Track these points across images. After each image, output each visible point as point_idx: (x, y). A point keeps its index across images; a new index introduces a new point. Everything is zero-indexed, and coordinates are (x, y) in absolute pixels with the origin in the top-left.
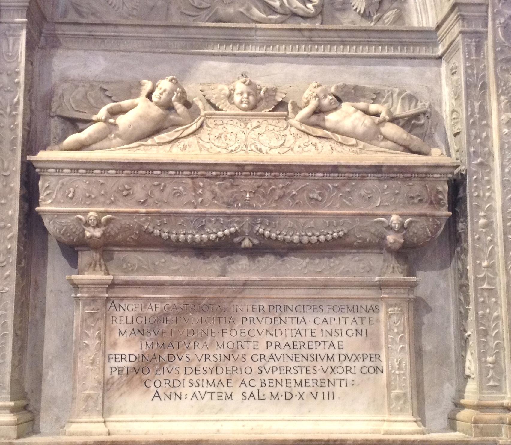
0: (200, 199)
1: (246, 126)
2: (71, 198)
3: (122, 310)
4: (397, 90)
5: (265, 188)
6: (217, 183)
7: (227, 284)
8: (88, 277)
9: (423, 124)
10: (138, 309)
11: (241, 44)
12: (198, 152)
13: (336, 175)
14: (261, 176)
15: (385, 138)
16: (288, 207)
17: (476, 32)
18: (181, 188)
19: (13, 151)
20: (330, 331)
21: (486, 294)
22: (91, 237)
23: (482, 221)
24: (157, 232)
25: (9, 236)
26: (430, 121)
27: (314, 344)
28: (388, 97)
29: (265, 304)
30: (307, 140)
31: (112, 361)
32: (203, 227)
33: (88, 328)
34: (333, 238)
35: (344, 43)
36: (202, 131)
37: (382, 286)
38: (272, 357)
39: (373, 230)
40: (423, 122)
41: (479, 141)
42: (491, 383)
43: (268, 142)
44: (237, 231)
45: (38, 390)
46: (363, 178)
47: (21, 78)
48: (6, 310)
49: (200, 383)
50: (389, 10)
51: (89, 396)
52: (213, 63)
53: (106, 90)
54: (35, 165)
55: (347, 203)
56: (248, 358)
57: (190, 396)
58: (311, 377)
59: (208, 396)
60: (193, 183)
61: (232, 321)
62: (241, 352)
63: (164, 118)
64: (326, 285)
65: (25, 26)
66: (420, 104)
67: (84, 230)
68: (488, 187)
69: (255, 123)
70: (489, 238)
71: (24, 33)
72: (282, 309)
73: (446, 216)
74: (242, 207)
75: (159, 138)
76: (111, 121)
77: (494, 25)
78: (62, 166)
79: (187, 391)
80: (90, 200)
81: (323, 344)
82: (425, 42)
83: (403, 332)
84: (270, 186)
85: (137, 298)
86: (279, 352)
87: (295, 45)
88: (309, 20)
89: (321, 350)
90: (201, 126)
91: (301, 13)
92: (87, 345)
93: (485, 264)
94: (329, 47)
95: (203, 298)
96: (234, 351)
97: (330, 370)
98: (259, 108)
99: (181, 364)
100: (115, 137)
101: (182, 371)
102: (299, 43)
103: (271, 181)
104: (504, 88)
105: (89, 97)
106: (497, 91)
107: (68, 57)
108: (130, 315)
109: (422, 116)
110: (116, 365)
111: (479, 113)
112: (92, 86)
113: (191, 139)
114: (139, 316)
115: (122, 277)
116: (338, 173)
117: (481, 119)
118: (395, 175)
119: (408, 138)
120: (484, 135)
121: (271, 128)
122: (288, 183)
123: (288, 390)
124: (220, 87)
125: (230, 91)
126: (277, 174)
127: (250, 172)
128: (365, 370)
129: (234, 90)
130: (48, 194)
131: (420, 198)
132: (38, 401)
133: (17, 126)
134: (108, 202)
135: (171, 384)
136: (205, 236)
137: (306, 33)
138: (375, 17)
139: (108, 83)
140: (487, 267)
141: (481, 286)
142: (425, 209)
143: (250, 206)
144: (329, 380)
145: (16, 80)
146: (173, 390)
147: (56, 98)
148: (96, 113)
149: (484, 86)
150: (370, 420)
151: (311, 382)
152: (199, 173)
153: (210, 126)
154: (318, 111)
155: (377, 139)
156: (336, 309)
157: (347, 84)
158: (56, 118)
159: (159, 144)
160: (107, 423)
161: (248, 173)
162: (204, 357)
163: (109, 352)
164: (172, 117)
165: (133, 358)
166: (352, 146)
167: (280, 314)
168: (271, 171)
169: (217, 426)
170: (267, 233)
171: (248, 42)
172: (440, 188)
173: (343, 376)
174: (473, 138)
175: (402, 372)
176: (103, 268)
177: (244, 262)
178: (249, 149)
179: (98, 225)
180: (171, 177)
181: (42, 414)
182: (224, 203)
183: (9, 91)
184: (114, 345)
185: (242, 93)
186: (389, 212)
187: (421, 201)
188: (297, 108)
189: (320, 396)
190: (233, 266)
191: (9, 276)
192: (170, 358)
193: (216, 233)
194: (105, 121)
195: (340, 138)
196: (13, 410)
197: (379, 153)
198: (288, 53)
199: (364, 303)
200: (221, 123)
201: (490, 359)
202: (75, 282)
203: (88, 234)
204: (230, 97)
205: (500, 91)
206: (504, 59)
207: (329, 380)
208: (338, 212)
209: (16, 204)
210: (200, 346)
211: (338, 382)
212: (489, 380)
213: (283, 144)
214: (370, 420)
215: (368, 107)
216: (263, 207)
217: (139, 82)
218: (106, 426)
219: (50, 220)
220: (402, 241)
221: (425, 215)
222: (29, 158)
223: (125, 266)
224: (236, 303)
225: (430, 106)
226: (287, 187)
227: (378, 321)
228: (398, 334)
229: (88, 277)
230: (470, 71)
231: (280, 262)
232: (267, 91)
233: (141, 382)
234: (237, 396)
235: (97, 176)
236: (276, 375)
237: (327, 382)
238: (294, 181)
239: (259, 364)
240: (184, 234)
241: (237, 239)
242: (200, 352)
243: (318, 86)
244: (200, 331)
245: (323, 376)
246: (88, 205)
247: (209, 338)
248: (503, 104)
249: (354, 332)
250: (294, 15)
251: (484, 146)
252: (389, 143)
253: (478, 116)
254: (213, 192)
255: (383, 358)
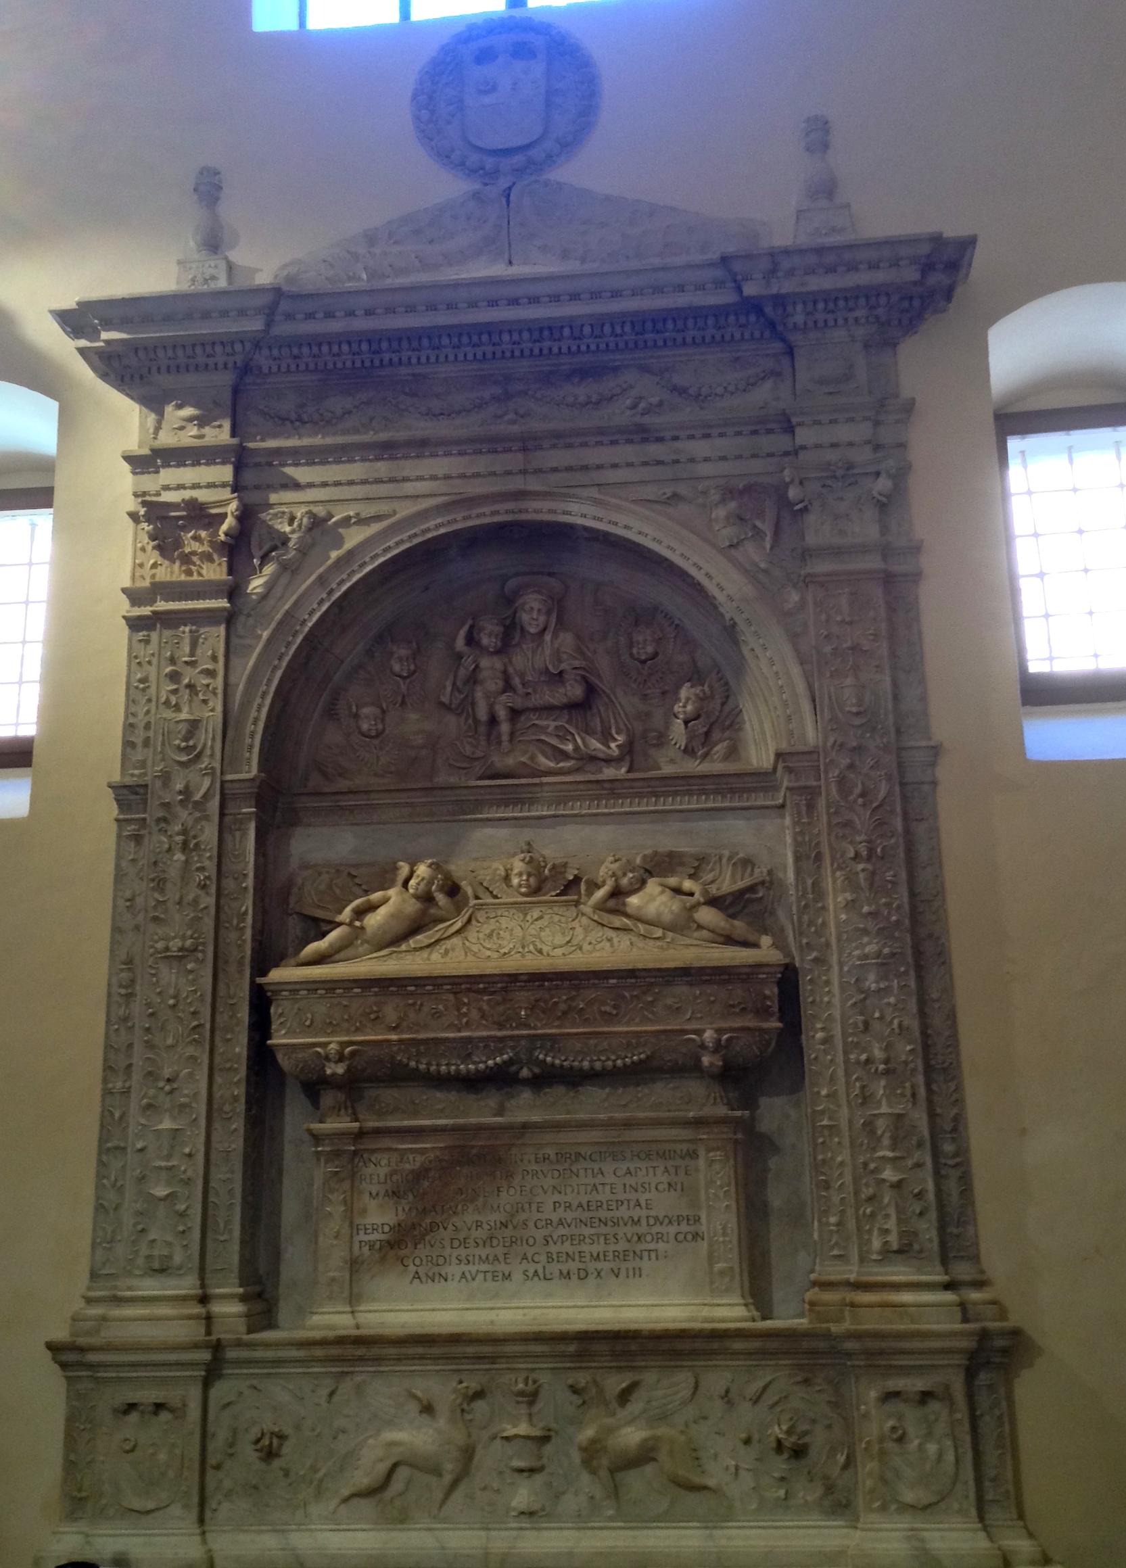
0: (465, 1020)
1: (525, 917)
2: (309, 1026)
3: (373, 1166)
4: (726, 853)
5: (546, 1002)
6: (486, 998)
7: (510, 1127)
8: (331, 1125)
9: (761, 898)
10: (393, 1164)
11: (523, 803)
12: (462, 957)
13: (633, 981)
14: (539, 986)
15: (700, 927)
16: (574, 1025)
17: (805, 787)
18: (441, 1007)
19: (241, 972)
20: (634, 1185)
21: (826, 1132)
22: (333, 1074)
23: (820, 1035)
24: (413, 1064)
25: (235, 1080)
26: (771, 892)
27: (614, 1203)
28: (715, 863)
29: (550, 1151)
30: (600, 934)
31: (362, 1232)
32: (469, 1055)
33: (332, 1191)
34: (633, 1062)
35: (656, 795)
36: (470, 927)
37: (698, 1123)
38: (561, 1223)
39: (684, 1050)
40: (760, 894)
41: (813, 929)
42: (835, 1252)
43: (551, 938)
44: (511, 1059)
45: (275, 1272)
46: (668, 983)
47: (250, 882)
48: (232, 1172)
49: (471, 1258)
50: (721, 741)
51: (333, 1279)
52: (489, 831)
53: (355, 877)
54: (266, 988)
55: (650, 1016)
56: (531, 1224)
57: (457, 1277)
58: (612, 1247)
59: (481, 1276)
60: (456, 998)
61: (509, 1176)
62: (522, 1216)
63: (423, 913)
64: (628, 1124)
65: (253, 817)
66: (757, 871)
67: (324, 1066)
68: (827, 989)
69: (536, 913)
70: (829, 1057)
71: (252, 825)
72: (573, 1158)
73: (777, 1028)
74: (517, 1028)
75: (416, 942)
76: (357, 924)
77: (826, 779)
78: (298, 987)
79: (454, 1270)
80: (331, 1027)
81: (626, 1202)
82: (762, 787)
83: (729, 1185)
84: (552, 998)
85: (389, 1149)
86: (569, 1216)
87: (592, 800)
88: (613, 763)
89: (623, 1212)
90: (469, 921)
91: (601, 755)
92: (330, 1214)
93: (824, 1092)
94: (637, 800)
95: (473, 1147)
96: (512, 1216)
97: (635, 1238)
98: (544, 891)
99: (445, 1235)
100: (362, 944)
101: (447, 1243)
102: (598, 798)
103: (554, 992)
104: (841, 861)
105: (334, 888)
106: (832, 865)
107: (309, 836)
108: (383, 1171)
109: (760, 887)
110: (366, 1238)
111: (813, 893)
112: (338, 871)
113: (456, 941)
114: (393, 1173)
115: (372, 1124)
116: (636, 977)
117: (816, 901)
118: (708, 978)
119: (728, 926)
120: (820, 921)
121: (556, 918)
122: (574, 993)
123: (581, 1266)
124: (495, 865)
125: (506, 870)
126: (559, 983)
127: (525, 982)
128: (681, 1237)
129: (512, 870)
130: (281, 1023)
131: (743, 1006)
132: (276, 1286)
133: (244, 941)
134: (353, 1029)
135: (434, 1261)
136: (471, 1066)
137: (607, 785)
138: (700, 753)
139: (357, 866)
140: (828, 1096)
141: (821, 1121)
142: (750, 1022)
143: (527, 1026)
144: (634, 1252)
145: (244, 885)
146: (436, 1269)
147: (295, 890)
148: (340, 912)
149: (819, 857)
150: (689, 1305)
151: (611, 1254)
152: (463, 986)
153: (480, 920)
154: (617, 893)
155: (689, 928)
156: (643, 1156)
157: (660, 850)
158: (295, 916)
159: (415, 949)
160: (356, 1314)
161: (523, 984)
162: (474, 1225)
163: (358, 1220)
164: (432, 911)
165: (386, 1229)
166: (658, 938)
167: (571, 1165)
168: (551, 980)
169: (491, 1315)
170: (549, 1059)
171: (532, 801)
172: (767, 992)
173: (652, 1246)
174: (805, 926)
175: (727, 1239)
176: (350, 1111)
177: (526, 1095)
178: (526, 950)
179: (341, 1058)
180: (429, 993)
181: (281, 1304)
182: (494, 1023)
183: (236, 899)
184: (364, 1211)
185: (520, 874)
186: (703, 1027)
187: (743, 1009)
188: (594, 886)
189: (623, 1273)
190: (513, 1102)
191: (236, 1130)
192: (433, 1227)
193: (486, 1062)
194: (350, 924)
195: (642, 928)
196: (243, 1299)
197: (691, 948)
198: (584, 812)
199: (678, 1147)
200: (493, 915)
201: (833, 1220)
202: (314, 1132)
203: (329, 1072)
204: (507, 878)
205: (835, 866)
206: (839, 823)
207: (634, 1252)
208: (639, 1029)
209: (244, 1038)
210: (470, 1210)
211: (645, 1254)
212: (832, 1248)
213: (569, 942)
214: (689, 1305)
215: (681, 883)
216: (542, 1027)
217: (395, 863)
218: (354, 1318)
219: (285, 1055)
220: (721, 1063)
221: (748, 1029)
222: (260, 980)
223: (377, 1107)
224: (514, 1151)
225: (770, 872)
226: (572, 999)
227: (697, 1170)
228: (721, 1187)
229: (331, 1125)
230: (800, 839)
231: (572, 1094)
232: (554, 867)
233: (398, 1259)
234: (518, 1276)
235: (340, 996)
236: (567, 1247)
237: (632, 1254)
238: (582, 991)
239: (544, 1232)
240: (447, 1065)
241: (513, 1068)
242: (470, 1217)
243: (616, 861)
244: (470, 1191)
245: (627, 1246)
246: (329, 1035)
247: (481, 1199)
248: (839, 882)
249: (666, 1186)
250: (593, 759)
251: (820, 937)
252: (705, 933)
253: (811, 896)
254: (480, 1009)
255: (704, 1220)
